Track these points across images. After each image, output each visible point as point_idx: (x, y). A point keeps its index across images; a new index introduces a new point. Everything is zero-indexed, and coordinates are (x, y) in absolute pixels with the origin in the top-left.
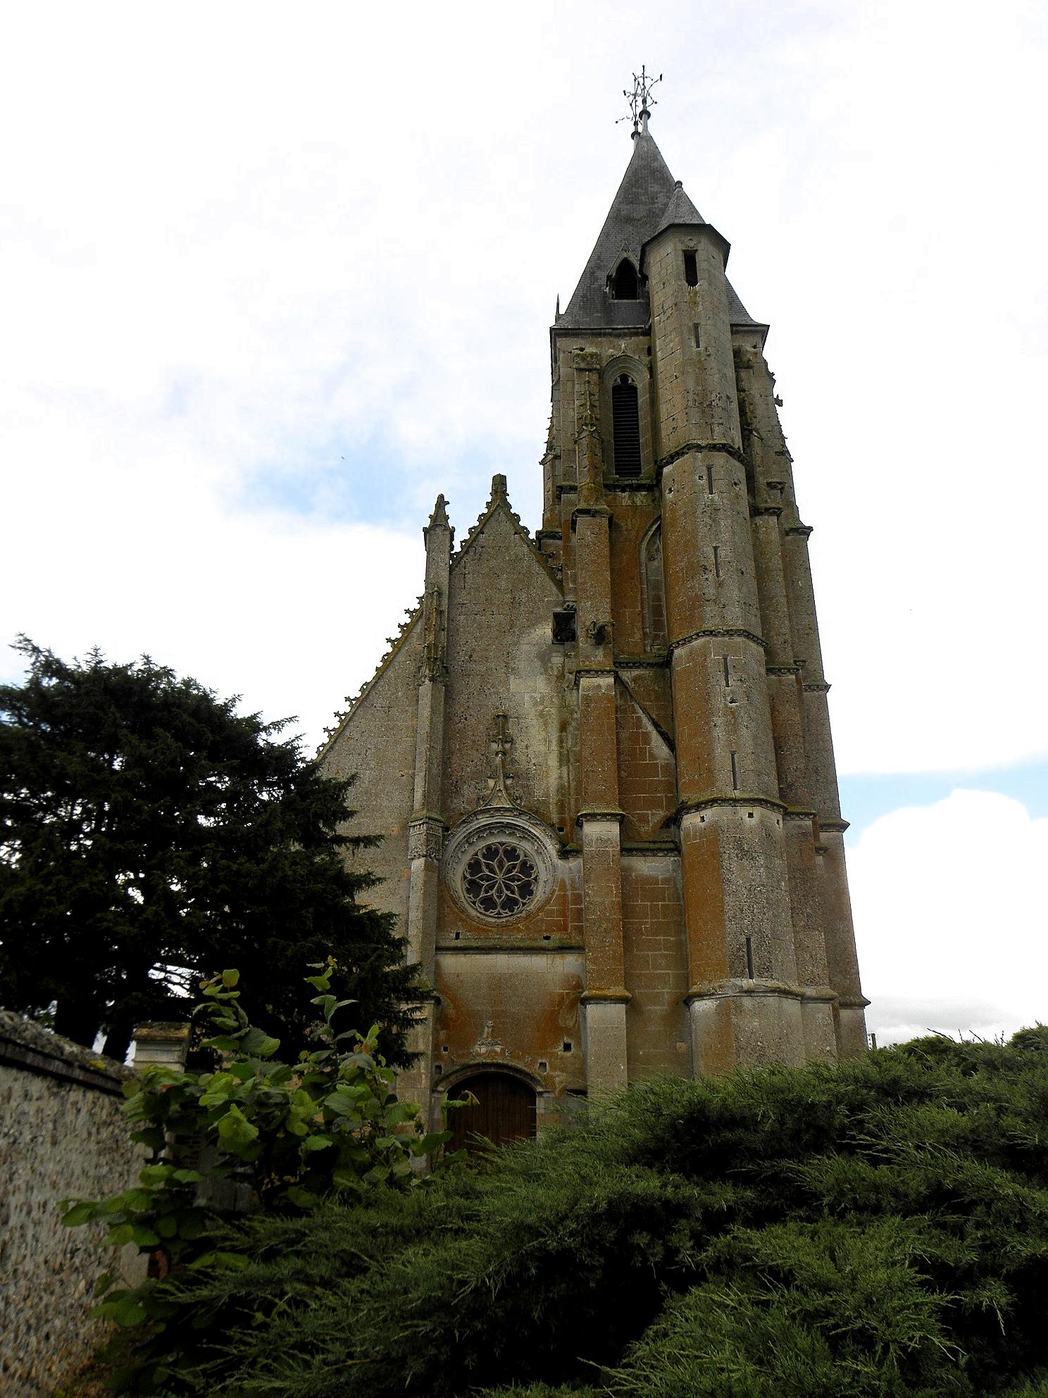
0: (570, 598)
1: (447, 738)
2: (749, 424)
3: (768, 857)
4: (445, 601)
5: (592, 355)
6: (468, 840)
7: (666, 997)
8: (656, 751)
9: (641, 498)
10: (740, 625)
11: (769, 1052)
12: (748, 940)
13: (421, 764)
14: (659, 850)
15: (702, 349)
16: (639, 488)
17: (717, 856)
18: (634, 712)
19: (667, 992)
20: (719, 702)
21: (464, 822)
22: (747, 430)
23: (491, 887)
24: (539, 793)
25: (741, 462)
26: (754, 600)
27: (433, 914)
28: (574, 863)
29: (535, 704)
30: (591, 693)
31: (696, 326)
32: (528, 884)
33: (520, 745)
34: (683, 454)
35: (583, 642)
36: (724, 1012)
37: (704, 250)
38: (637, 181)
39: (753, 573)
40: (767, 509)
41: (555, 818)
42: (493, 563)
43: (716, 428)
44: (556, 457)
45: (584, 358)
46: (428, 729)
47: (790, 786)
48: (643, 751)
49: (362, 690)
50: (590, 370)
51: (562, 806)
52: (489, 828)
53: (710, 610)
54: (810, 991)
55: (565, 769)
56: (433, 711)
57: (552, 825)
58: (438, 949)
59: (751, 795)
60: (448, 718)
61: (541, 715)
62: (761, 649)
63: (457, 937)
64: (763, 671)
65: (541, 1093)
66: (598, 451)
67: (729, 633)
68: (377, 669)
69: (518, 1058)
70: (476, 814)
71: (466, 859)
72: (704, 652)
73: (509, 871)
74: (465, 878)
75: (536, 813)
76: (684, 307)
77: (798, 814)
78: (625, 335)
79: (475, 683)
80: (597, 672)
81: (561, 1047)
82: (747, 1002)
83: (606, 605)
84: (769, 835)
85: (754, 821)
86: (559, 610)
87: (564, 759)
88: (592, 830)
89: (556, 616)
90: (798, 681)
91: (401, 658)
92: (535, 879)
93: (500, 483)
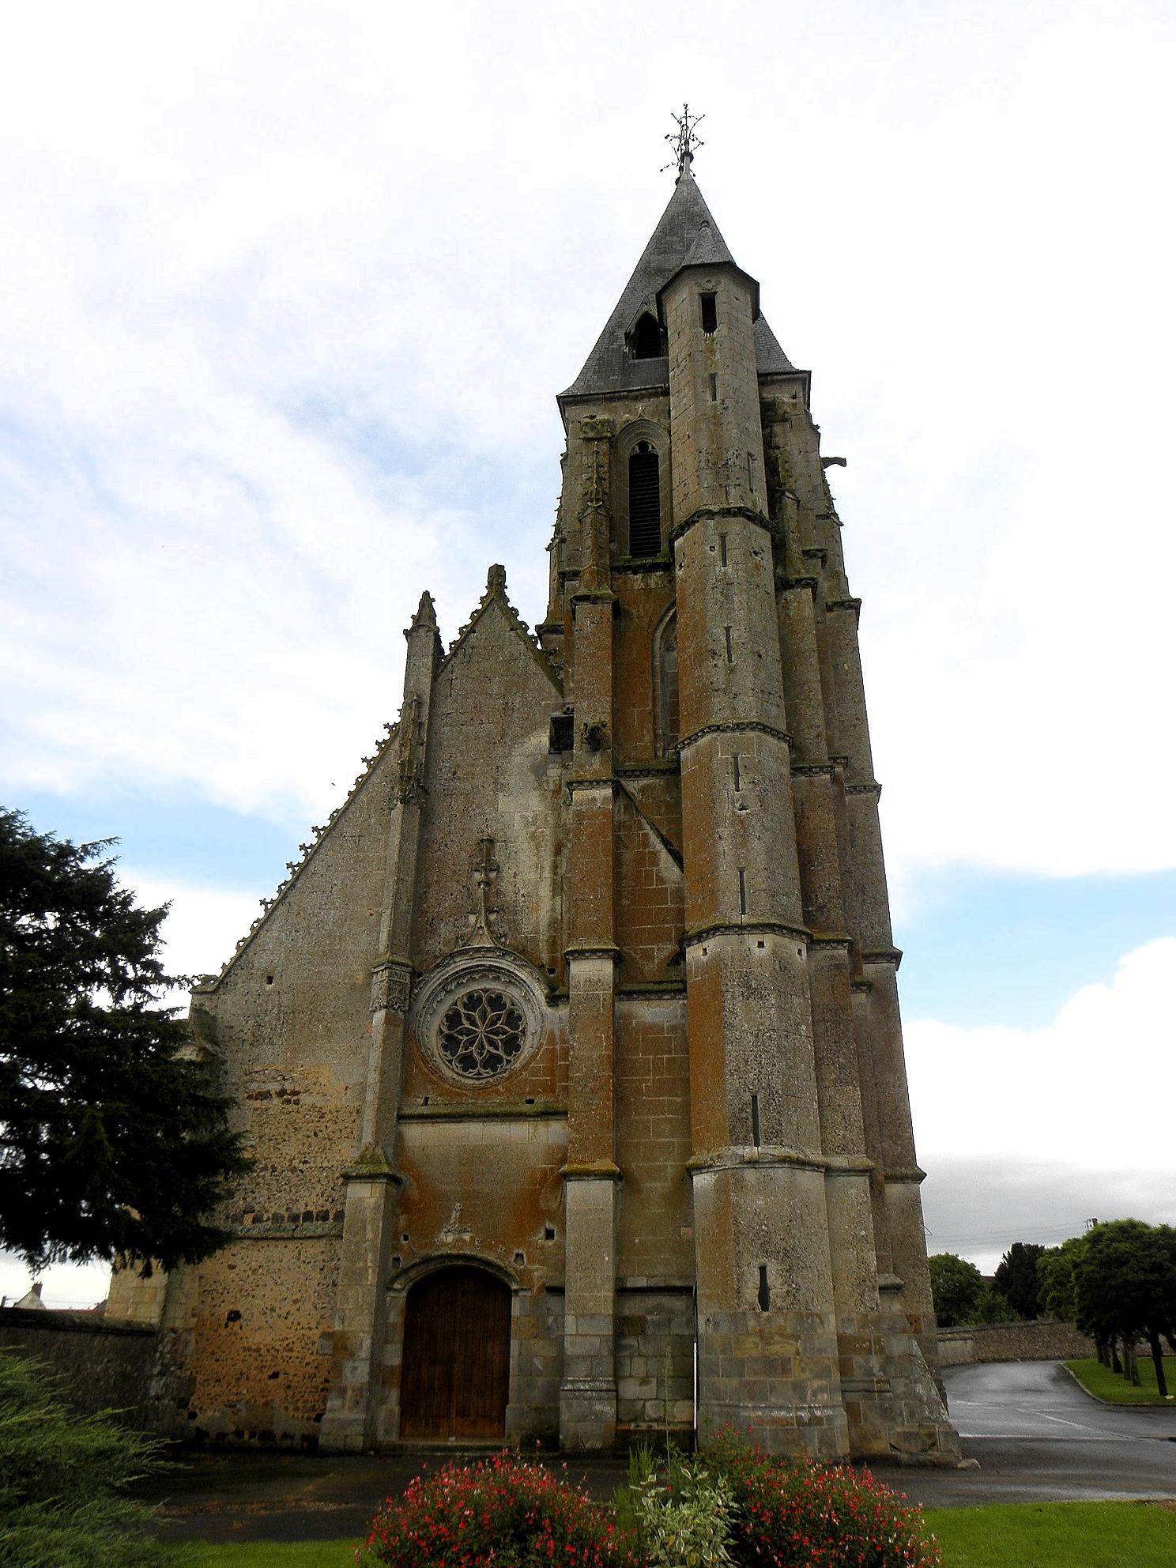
0: (569, 699)
2: (780, 485)
3: (780, 993)
4: (426, 711)
5: (603, 423)
6: (444, 986)
7: (669, 1170)
8: (665, 874)
9: (655, 579)
10: (753, 717)
11: (776, 1239)
12: (754, 1098)
13: (388, 900)
14: (664, 992)
15: (718, 402)
16: (654, 568)
17: (718, 995)
18: (641, 828)
19: (670, 1166)
20: (726, 810)
21: (438, 966)
22: (775, 492)
24: (527, 929)
25: (765, 527)
26: (777, 687)
28: (563, 1011)
29: (527, 825)
31: (713, 377)
32: (515, 1038)
33: (507, 874)
34: (694, 523)
35: (579, 749)
36: (722, 1188)
37: (726, 292)
38: (672, 229)
39: (777, 656)
40: (798, 581)
41: (545, 957)
42: (485, 665)
43: (732, 491)
44: (563, 541)
45: (593, 427)
47: (821, 908)
48: (649, 875)
49: (332, 817)
50: (599, 439)
51: (553, 943)
52: (469, 972)
53: (719, 702)
54: (838, 1161)
55: (558, 899)
56: (404, 837)
58: (402, 1117)
59: (761, 920)
60: (424, 846)
61: (533, 837)
62: (785, 746)
63: (426, 1102)
64: (786, 770)
65: (516, 1291)
66: (604, 529)
67: (739, 727)
68: (350, 793)
69: (490, 1248)
70: (452, 955)
71: (444, 1009)
72: (710, 752)
73: (494, 1023)
74: (442, 1032)
76: (699, 356)
77: (828, 942)
78: (643, 397)
80: (591, 782)
81: (542, 1234)
82: (750, 1175)
83: (606, 704)
84: (783, 968)
85: (764, 952)
86: (558, 714)
87: (557, 888)
88: (580, 970)
89: (555, 721)
90: (835, 780)
91: (375, 779)
92: (523, 1032)
93: (497, 576)
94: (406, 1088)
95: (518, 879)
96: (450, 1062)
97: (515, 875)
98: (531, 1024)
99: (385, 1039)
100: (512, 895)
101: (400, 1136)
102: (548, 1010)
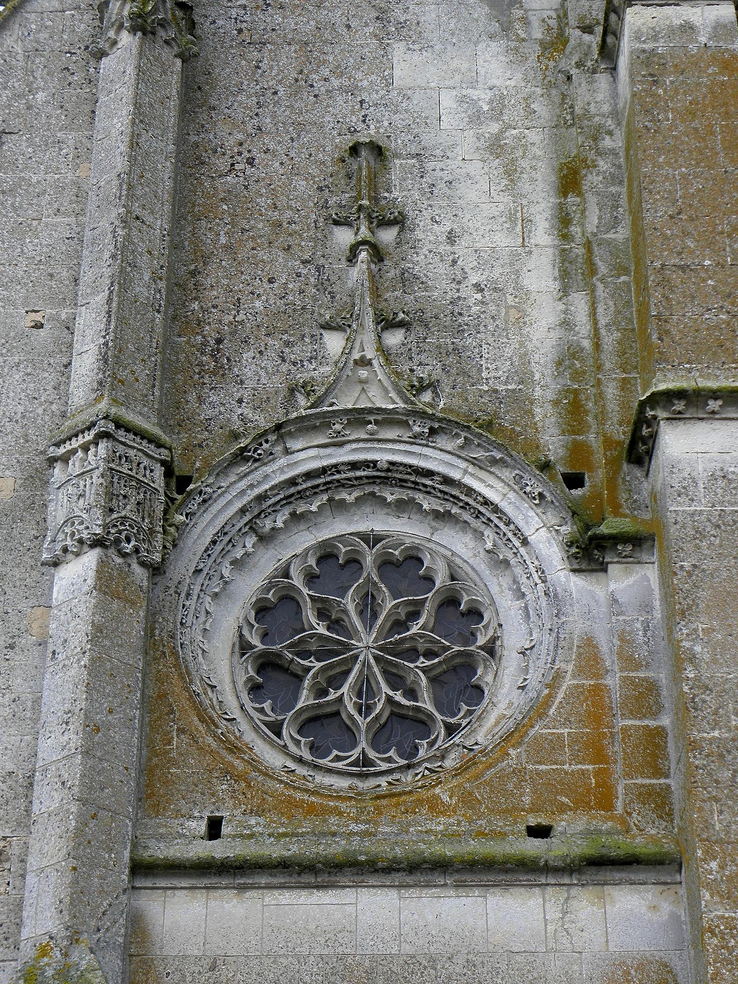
1: (186, 209)
6: (254, 521)
13: (98, 271)
21: (241, 456)
23: (336, 681)
27: (126, 740)
29: (477, 118)
30: (661, 47)
32: (464, 666)
33: (428, 233)
41: (553, 444)
46: (120, 164)
52: (324, 481)
55: (579, 303)
56: (141, 116)
57: (545, 466)
58: (143, 869)
60: (191, 160)
61: (495, 147)
63: (214, 829)
71: (250, 585)
73: (400, 625)
75: (488, 431)
79: (282, 63)
87: (575, 270)
92: (490, 649)
94: (152, 790)
95: (460, 249)
96: (276, 728)
97: (451, 238)
98: (511, 620)
99: (98, 633)
100: (444, 284)
101: (138, 926)
102: (576, 584)
